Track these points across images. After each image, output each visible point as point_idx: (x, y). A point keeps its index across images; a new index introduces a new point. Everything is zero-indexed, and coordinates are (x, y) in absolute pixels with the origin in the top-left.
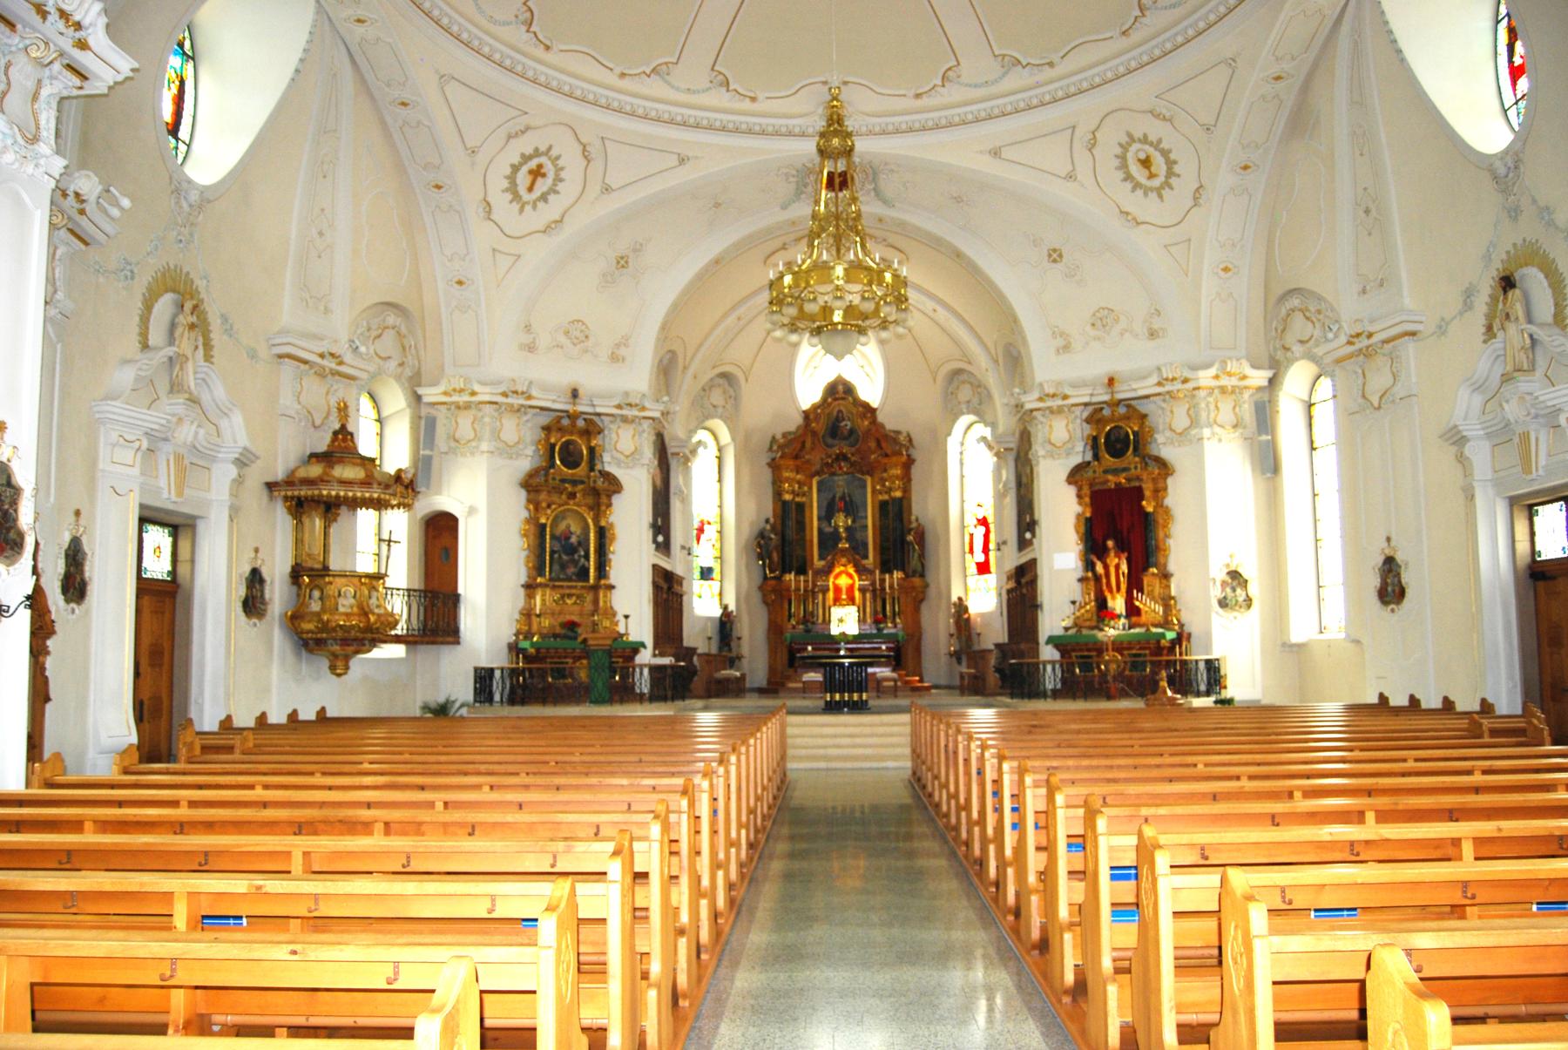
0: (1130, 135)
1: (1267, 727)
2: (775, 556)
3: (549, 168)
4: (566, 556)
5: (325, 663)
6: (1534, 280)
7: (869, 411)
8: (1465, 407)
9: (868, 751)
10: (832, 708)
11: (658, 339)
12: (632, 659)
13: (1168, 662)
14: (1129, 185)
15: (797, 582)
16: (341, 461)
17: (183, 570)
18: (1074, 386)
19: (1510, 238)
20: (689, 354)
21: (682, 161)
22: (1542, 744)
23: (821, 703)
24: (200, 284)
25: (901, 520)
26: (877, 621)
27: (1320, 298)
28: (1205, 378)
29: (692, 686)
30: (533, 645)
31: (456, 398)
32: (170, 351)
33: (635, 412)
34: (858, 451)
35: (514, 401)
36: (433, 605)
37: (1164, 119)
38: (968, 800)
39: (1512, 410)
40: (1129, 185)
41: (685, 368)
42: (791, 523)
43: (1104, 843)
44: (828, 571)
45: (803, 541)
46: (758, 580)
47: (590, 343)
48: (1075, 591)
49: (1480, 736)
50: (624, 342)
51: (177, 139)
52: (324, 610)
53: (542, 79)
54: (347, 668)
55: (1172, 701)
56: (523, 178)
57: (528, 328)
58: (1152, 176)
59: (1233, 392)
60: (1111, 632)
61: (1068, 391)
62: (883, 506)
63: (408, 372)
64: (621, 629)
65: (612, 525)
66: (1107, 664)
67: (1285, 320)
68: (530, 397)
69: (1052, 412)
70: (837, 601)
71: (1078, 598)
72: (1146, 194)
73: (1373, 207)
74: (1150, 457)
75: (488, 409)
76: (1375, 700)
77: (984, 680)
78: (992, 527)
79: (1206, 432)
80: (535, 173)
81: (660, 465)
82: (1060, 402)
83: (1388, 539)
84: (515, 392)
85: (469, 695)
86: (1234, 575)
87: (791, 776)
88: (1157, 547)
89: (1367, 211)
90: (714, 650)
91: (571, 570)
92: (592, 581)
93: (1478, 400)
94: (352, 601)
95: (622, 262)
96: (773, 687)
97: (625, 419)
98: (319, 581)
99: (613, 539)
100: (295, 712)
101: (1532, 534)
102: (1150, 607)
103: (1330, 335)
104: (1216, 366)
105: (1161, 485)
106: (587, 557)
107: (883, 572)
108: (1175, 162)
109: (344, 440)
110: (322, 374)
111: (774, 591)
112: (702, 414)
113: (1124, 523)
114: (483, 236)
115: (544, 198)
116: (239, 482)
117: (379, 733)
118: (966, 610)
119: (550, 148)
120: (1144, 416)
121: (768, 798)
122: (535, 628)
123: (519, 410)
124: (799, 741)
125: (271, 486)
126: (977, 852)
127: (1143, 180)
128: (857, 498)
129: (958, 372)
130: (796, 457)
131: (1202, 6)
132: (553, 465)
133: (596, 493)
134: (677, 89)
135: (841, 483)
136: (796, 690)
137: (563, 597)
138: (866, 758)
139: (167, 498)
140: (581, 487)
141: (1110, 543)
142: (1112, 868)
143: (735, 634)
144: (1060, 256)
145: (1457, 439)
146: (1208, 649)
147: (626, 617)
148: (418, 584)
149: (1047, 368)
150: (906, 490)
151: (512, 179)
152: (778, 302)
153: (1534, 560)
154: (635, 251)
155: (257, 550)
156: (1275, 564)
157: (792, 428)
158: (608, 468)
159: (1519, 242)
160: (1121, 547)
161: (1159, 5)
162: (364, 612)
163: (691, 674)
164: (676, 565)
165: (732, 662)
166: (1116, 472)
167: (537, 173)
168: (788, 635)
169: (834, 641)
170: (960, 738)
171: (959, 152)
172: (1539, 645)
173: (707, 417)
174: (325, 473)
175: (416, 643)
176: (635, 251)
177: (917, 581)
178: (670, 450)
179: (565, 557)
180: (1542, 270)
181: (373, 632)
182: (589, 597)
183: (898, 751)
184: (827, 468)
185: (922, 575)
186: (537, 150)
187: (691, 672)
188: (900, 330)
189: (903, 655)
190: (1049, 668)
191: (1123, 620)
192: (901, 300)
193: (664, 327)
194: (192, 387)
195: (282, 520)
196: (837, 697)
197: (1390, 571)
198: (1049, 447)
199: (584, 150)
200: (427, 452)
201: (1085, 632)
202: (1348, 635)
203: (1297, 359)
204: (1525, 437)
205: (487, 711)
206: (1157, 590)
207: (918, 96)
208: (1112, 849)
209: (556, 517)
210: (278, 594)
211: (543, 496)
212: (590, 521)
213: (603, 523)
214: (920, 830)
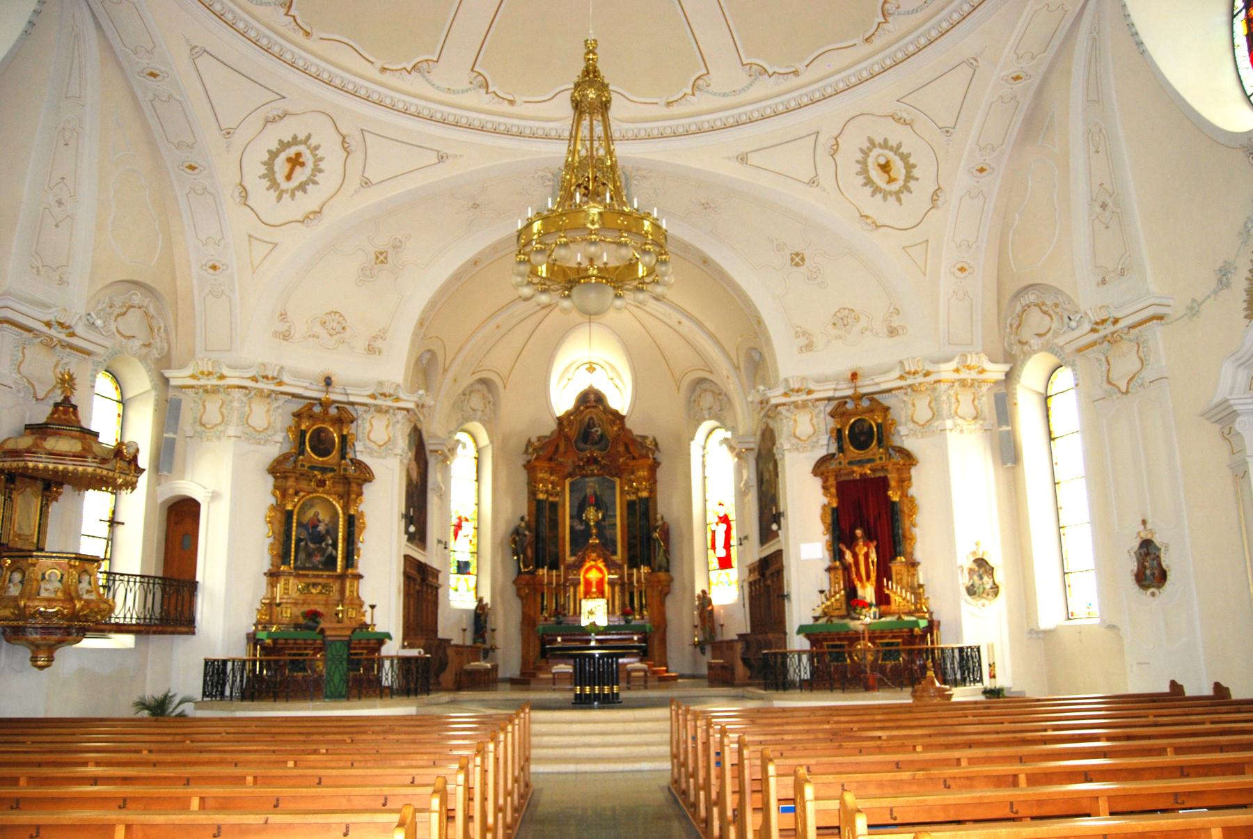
0: (871, 141)
3: (307, 157)
4: (312, 544)
7: (618, 418)
10: (582, 702)
11: (415, 335)
13: (920, 651)
14: (869, 190)
15: (550, 577)
16: (57, 433)
20: (448, 362)
21: (442, 158)
23: (571, 696)
26: (625, 614)
27: (1058, 291)
28: (946, 371)
30: (270, 635)
31: (203, 382)
33: (389, 403)
34: (608, 455)
35: (265, 387)
37: (905, 123)
38: (696, 768)
40: (869, 190)
41: (445, 370)
42: (545, 521)
43: (811, 807)
44: (578, 566)
45: (556, 538)
46: (513, 574)
47: (347, 334)
48: (824, 581)
50: (382, 335)
52: (22, 595)
53: (301, 64)
54: (51, 659)
56: (281, 166)
57: (283, 316)
59: (972, 385)
61: (812, 386)
62: (631, 506)
63: (155, 354)
65: (362, 514)
67: (1020, 316)
68: (281, 383)
70: (587, 594)
71: (826, 587)
72: (885, 198)
73: (1110, 202)
74: (894, 448)
75: (237, 394)
76: (1166, 688)
78: (733, 525)
79: (949, 423)
80: (294, 161)
82: (805, 397)
83: (1144, 522)
84: (266, 377)
86: (981, 562)
87: (535, 784)
88: (904, 536)
90: (469, 642)
91: (318, 559)
94: (59, 585)
95: (381, 258)
96: (524, 680)
97: (379, 409)
98: (23, 563)
102: (899, 597)
103: (1073, 324)
104: (957, 359)
106: (335, 546)
107: (630, 567)
108: (914, 166)
109: (65, 412)
110: (49, 344)
113: (870, 512)
114: (238, 221)
115: (302, 187)
119: (309, 137)
120: (887, 409)
123: (270, 395)
126: (703, 813)
127: (883, 185)
129: (701, 381)
131: (947, 5)
132: (302, 451)
133: (346, 480)
134: (438, 88)
135: (592, 486)
137: (308, 585)
138: (619, 759)
140: (330, 475)
141: (859, 532)
142: (818, 828)
143: (489, 626)
144: (803, 259)
147: (373, 607)
148: (155, 570)
149: (789, 365)
150: (652, 491)
151: (269, 164)
157: (548, 433)
158: (360, 457)
160: (869, 537)
161: (902, 10)
162: (70, 597)
163: (441, 666)
164: (431, 557)
166: (861, 463)
167: (296, 161)
168: (540, 627)
169: (585, 631)
170: (689, 717)
171: (706, 157)
173: (467, 419)
175: (148, 633)
176: (395, 247)
177: (662, 575)
178: (429, 448)
179: (312, 546)
181: (91, 620)
182: (336, 587)
183: (654, 749)
184: (579, 471)
185: (667, 570)
186: (295, 137)
189: (650, 645)
191: (873, 609)
193: (421, 323)
197: (1147, 554)
198: (794, 441)
199: (344, 141)
202: (1103, 621)
203: (1035, 352)
207: (669, 104)
209: (304, 504)
211: (291, 482)
213: (352, 512)
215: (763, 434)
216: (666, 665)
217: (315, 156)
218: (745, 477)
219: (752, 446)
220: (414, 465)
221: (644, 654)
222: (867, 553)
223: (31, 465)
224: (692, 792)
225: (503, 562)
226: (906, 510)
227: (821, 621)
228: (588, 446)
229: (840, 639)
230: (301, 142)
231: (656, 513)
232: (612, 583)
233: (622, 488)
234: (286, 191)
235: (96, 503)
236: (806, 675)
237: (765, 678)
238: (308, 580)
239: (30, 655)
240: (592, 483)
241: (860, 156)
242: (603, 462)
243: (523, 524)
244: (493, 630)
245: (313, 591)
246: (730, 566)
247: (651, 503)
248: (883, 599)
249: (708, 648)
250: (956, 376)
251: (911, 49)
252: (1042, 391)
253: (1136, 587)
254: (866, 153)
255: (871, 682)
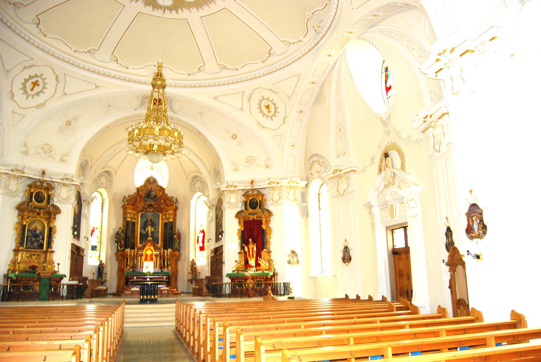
0: (263, 97)
1: (303, 310)
2: (122, 242)
6: (394, 154)
7: (162, 189)
8: (372, 197)
10: (143, 302)
11: (81, 155)
12: (60, 281)
13: (270, 284)
15: (131, 252)
18: (239, 183)
19: (386, 141)
20: (93, 163)
23: (139, 299)
26: (161, 268)
27: (324, 158)
29: (85, 293)
33: (69, 182)
34: (157, 204)
35: (16, 173)
39: (388, 197)
42: (130, 230)
44: (143, 248)
46: (115, 251)
47: (52, 153)
48: (237, 257)
49: (393, 311)
50: (67, 154)
55: (273, 298)
56: (29, 85)
57: (25, 145)
58: (269, 112)
60: (250, 272)
61: (237, 185)
62: (165, 225)
64: (56, 269)
65: (55, 227)
66: (249, 284)
67: (312, 164)
68: (23, 173)
69: (231, 192)
71: (238, 260)
72: (267, 118)
73: (342, 129)
74: (265, 209)
75: (4, 176)
76: (344, 297)
81: (78, 204)
83: (346, 240)
86: (293, 252)
88: (267, 242)
89: (340, 130)
90: (95, 278)
91: (36, 244)
92: (44, 249)
93: (376, 194)
95: (69, 123)
96: (119, 293)
97: (64, 185)
99: (55, 232)
102: (263, 264)
103: (327, 170)
104: (289, 178)
106: (43, 239)
107: (164, 249)
108: (278, 108)
111: (121, 255)
112: (97, 185)
113: (254, 233)
115: (38, 94)
118: (195, 264)
119: (42, 75)
122: (17, 268)
123: (18, 177)
124: (129, 315)
129: (196, 177)
130: (133, 205)
132: (31, 200)
133: (49, 213)
134: (97, 60)
135: (150, 215)
137: (31, 255)
140: (43, 211)
141: (250, 240)
143: (104, 272)
144: (236, 137)
145: (369, 206)
147: (59, 264)
149: (229, 176)
150: (175, 219)
152: (131, 140)
153: (394, 248)
154: (74, 119)
157: (132, 193)
158: (55, 204)
159: (390, 142)
160: (254, 242)
161: (275, 54)
163: (83, 289)
164: (81, 244)
165: (102, 283)
166: (253, 214)
167: (36, 84)
168: (126, 273)
171: (202, 96)
172: (396, 277)
177: (177, 253)
178: (82, 199)
179: (33, 239)
180: (397, 151)
182: (43, 256)
183: (170, 319)
185: (179, 251)
186: (36, 75)
187: (85, 287)
188: (179, 155)
190: (227, 286)
191: (254, 268)
192: (180, 144)
196: (145, 297)
197: (346, 251)
198: (229, 204)
199: (57, 77)
201: (240, 272)
203: (315, 178)
204: (392, 206)
206: (266, 257)
207: (189, 75)
209: (31, 222)
213: (51, 226)
214: (181, 355)
216: (177, 289)
217: (44, 82)
218: (211, 216)
220: (77, 207)
221: (168, 284)
222: (253, 247)
226: (268, 232)
228: (149, 200)
229: (242, 279)
230: (38, 77)
231: (175, 228)
232: (156, 256)
234: (31, 95)
236: (227, 292)
238: (31, 253)
240: (150, 216)
241: (258, 102)
242: (155, 206)
244: (106, 274)
245: (33, 257)
246: (204, 250)
248: (258, 265)
249: (194, 282)
250: (288, 185)
253: (342, 262)
255: (251, 294)
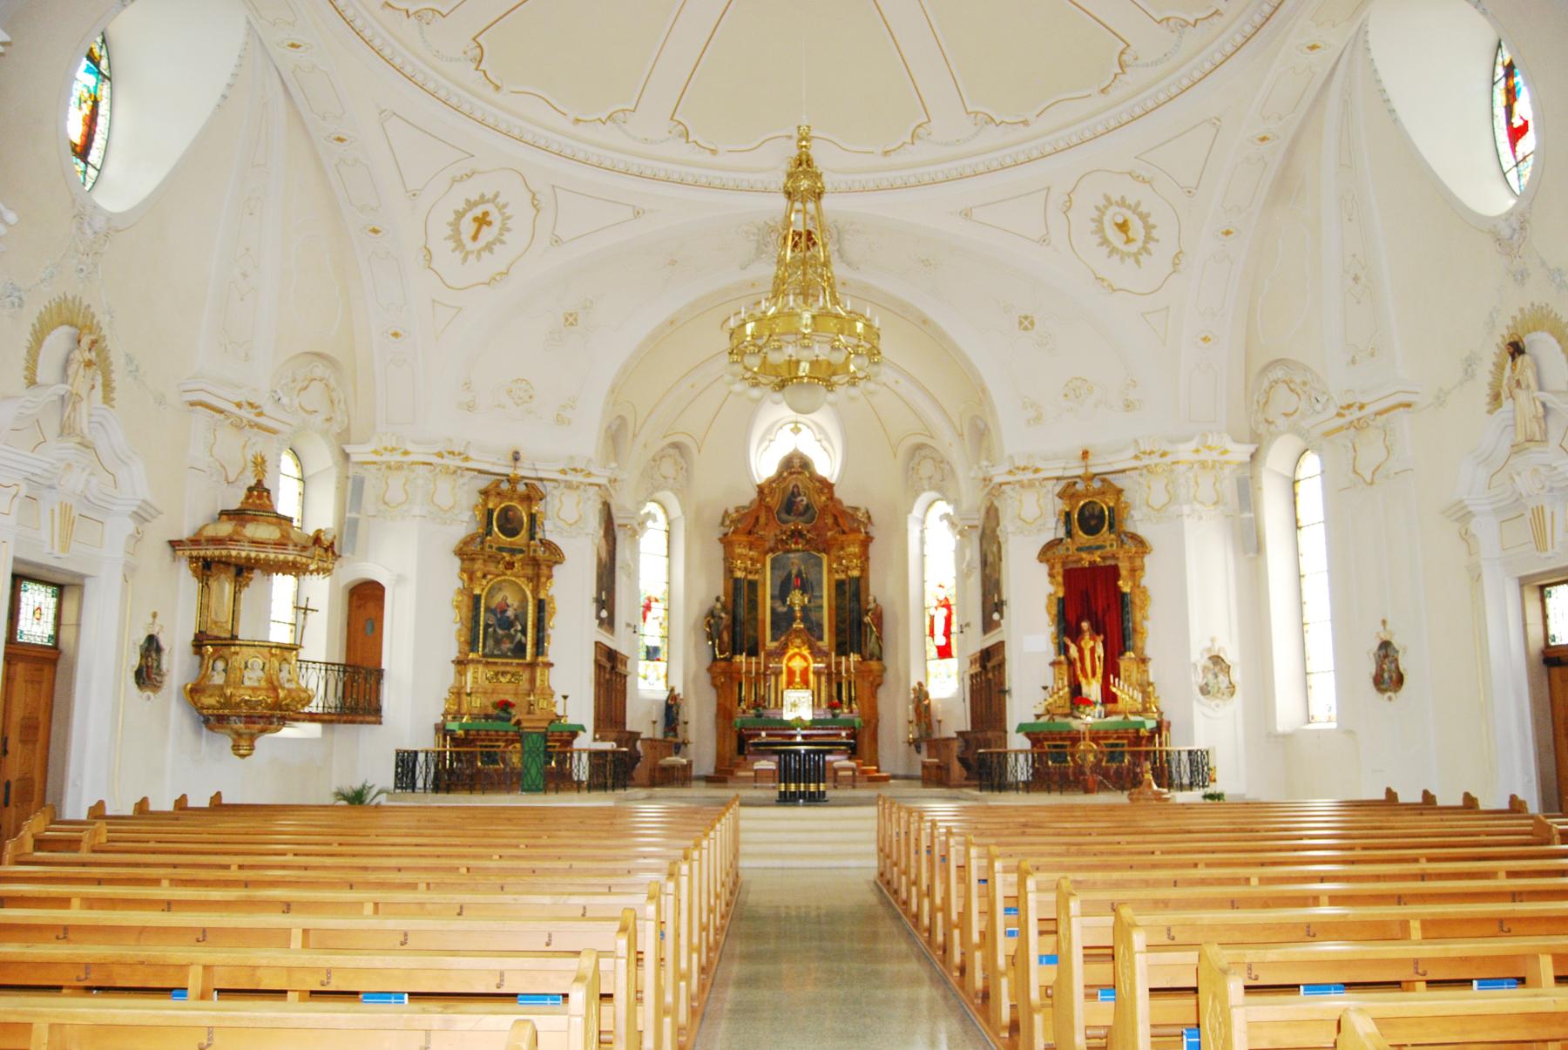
0: (1108, 199)
3: (495, 216)
4: (502, 634)
5: (227, 742)
7: (826, 486)
9: (828, 848)
10: (786, 799)
12: (570, 743)
13: (1148, 753)
16: (254, 519)
17: (67, 635)
22: (1548, 843)
23: (775, 794)
24: (102, 318)
25: (859, 601)
26: (832, 706)
28: (1185, 452)
29: (635, 774)
31: (387, 457)
32: (62, 389)
33: (580, 478)
34: (815, 528)
36: (353, 681)
37: (1144, 181)
42: (743, 602)
44: (781, 652)
46: (707, 661)
48: (1047, 676)
51: (87, 163)
52: (227, 684)
54: (252, 748)
55: (1158, 797)
57: (468, 385)
58: (1129, 241)
59: (1213, 467)
61: (1038, 464)
62: (840, 585)
63: (336, 428)
67: (1267, 393)
68: (467, 459)
70: (790, 683)
72: (1122, 259)
74: (1126, 534)
76: (1382, 796)
77: (948, 770)
79: (1186, 509)
83: (1384, 622)
85: (389, 780)
86: (1217, 660)
88: (1134, 630)
89: (1356, 279)
90: (659, 735)
91: (507, 646)
92: (529, 658)
94: (261, 674)
95: (571, 320)
96: (720, 777)
97: (569, 486)
98: (225, 651)
100: (144, 801)
101: (1545, 617)
102: (1126, 694)
103: (1318, 407)
104: (1197, 439)
105: (1138, 562)
106: (524, 632)
108: (1154, 227)
109: (260, 497)
110: (239, 426)
111: (724, 673)
113: (1097, 606)
115: (489, 247)
116: (137, 537)
117: (287, 823)
118: (926, 696)
119: (496, 196)
120: (1120, 491)
121: (721, 907)
122: (465, 708)
125: (174, 545)
128: (812, 577)
129: (920, 447)
132: (489, 532)
133: (535, 563)
135: (795, 561)
136: (746, 779)
137: (497, 674)
138: (825, 855)
139: (45, 553)
140: (520, 556)
141: (1085, 625)
143: (681, 718)
144: (1032, 324)
145: (1463, 515)
146: (1190, 740)
147: (565, 697)
148: (339, 657)
150: (864, 570)
151: (455, 226)
153: (1547, 646)
155: (155, 615)
156: (1263, 647)
157: (746, 503)
158: (549, 537)
160: (1097, 630)
162: (273, 687)
165: (678, 748)
166: (1090, 549)
167: (482, 221)
169: (788, 725)
172: (1555, 736)
173: (657, 488)
174: (237, 533)
175: (331, 722)
177: (874, 664)
178: (617, 522)
179: (500, 632)
180: (1552, 333)
182: (526, 675)
183: (861, 848)
185: (880, 659)
186: (483, 196)
187: (634, 758)
188: (871, 386)
189: (860, 743)
192: (874, 352)
194: (86, 431)
195: (187, 582)
197: (1386, 656)
198: (1019, 523)
200: (354, 515)
201: (1058, 719)
202: (1339, 725)
203: (1281, 433)
205: (408, 800)
206: (1135, 676)
207: (886, 153)
208: (1252, 1025)
209: (492, 589)
210: (178, 664)
211: (478, 565)
212: (529, 593)
213: (542, 596)
215: (988, 512)
219: (976, 523)
221: (853, 751)
222: (1093, 646)
223: (234, 553)
224: (903, 889)
225: (696, 645)
226: (1137, 601)
227: (1042, 720)
232: (818, 673)
233: (830, 566)
235: (283, 586)
236: (1022, 777)
237: (980, 778)
239: (231, 743)
240: (797, 566)
243: (719, 606)
247: (862, 582)
248: (1109, 697)
249: (924, 747)
251: (1150, 105)
252: (1290, 474)
253: (1374, 690)
254: (1101, 211)
255: (1090, 785)
